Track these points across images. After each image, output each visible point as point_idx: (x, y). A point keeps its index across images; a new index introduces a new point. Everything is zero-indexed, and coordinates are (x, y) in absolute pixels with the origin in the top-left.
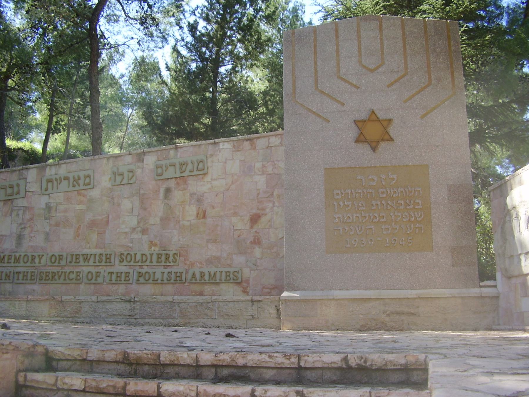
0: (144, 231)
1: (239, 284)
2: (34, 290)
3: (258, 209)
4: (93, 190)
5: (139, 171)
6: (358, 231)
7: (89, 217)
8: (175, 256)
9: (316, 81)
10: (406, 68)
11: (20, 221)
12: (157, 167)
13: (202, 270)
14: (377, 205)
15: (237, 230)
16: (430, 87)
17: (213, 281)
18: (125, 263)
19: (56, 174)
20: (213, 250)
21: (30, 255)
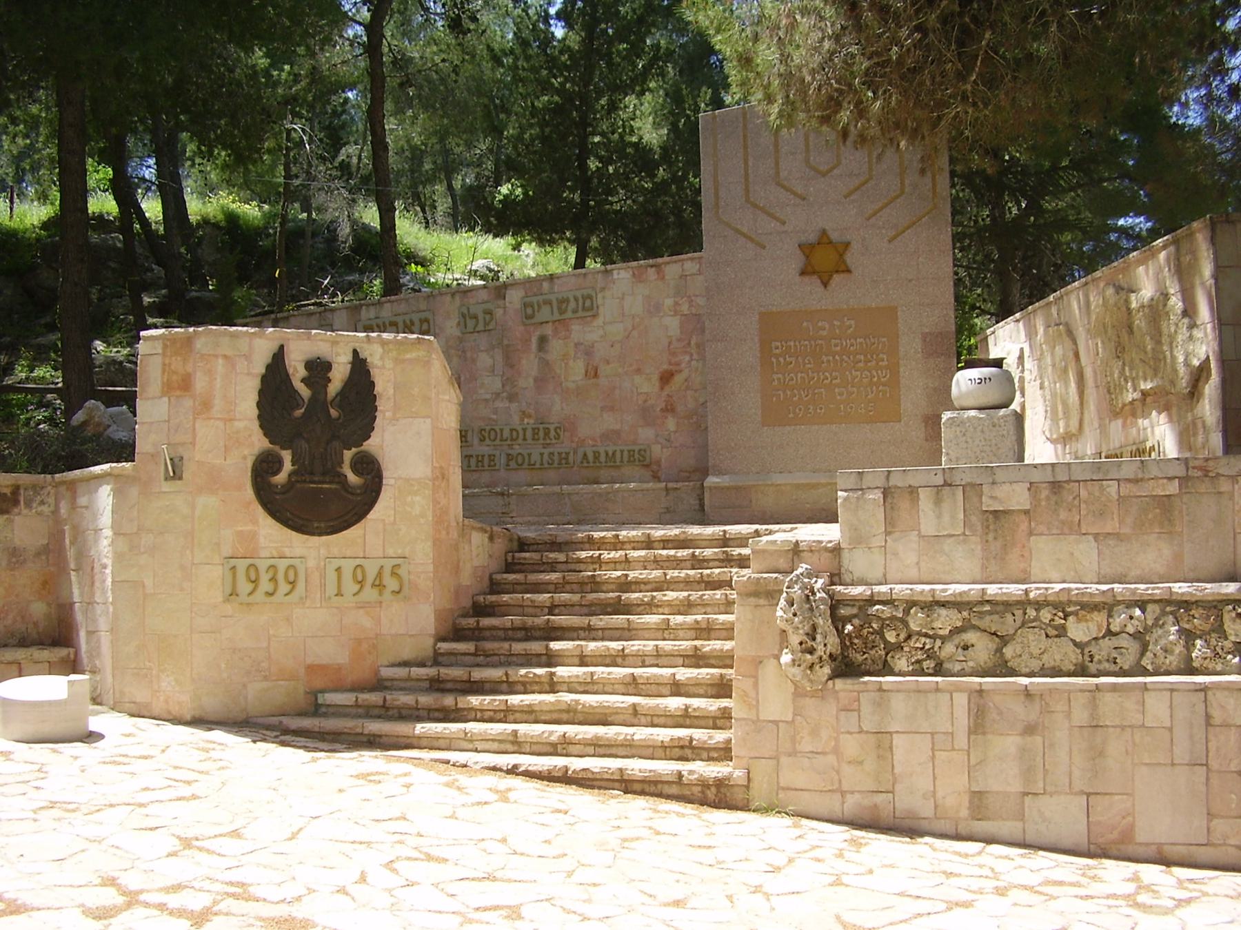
0: (512, 398)
1: (647, 466)
3: (670, 364)
9: (747, 190)
14: (829, 361)
18: (487, 442)
20: (609, 422)
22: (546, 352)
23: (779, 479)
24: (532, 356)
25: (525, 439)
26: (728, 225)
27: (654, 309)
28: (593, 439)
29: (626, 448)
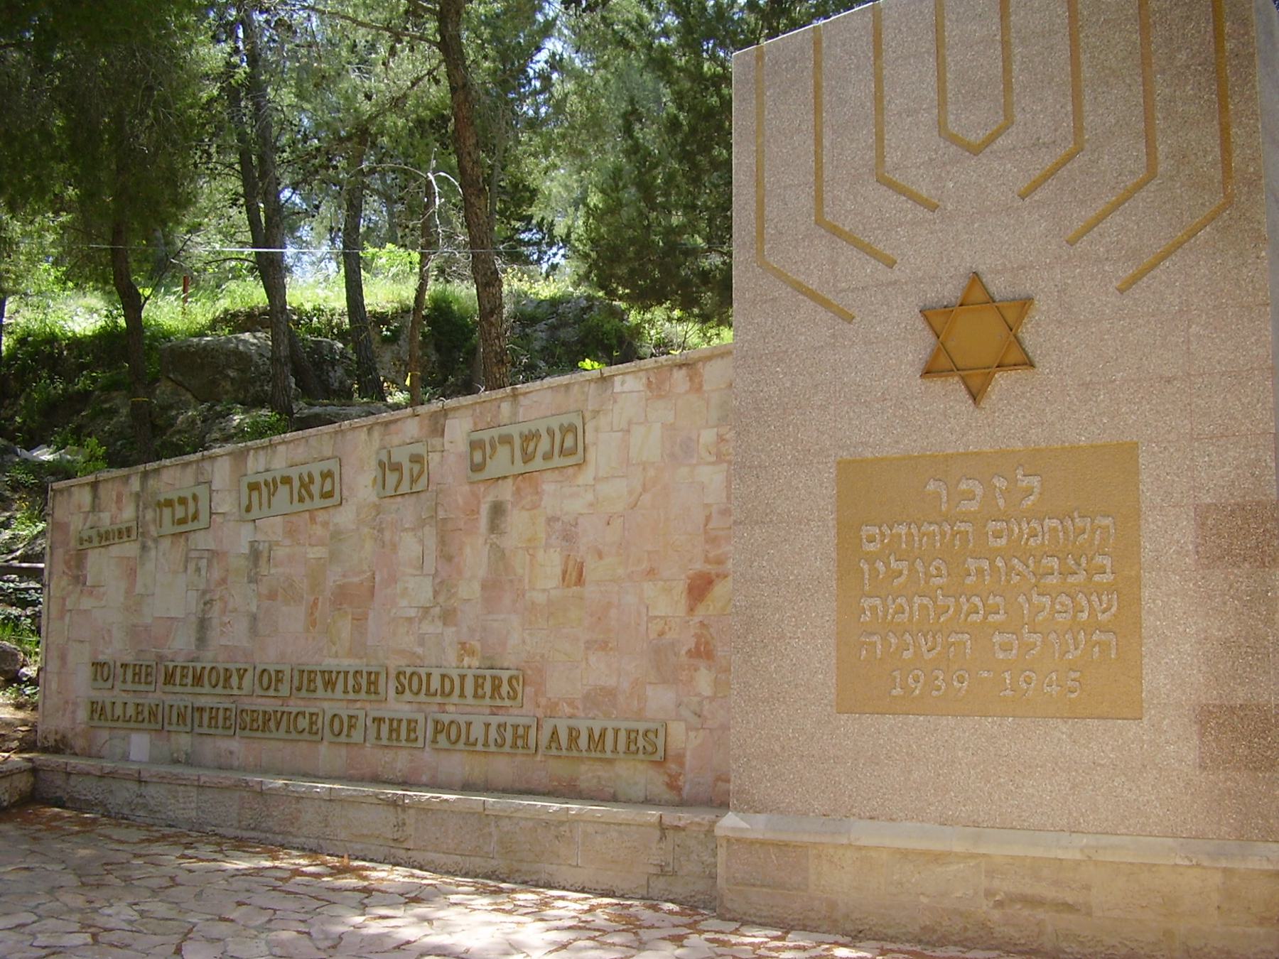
0: (448, 616)
1: (660, 764)
2: (231, 753)
3: (707, 561)
4: (341, 508)
5: (434, 458)
6: (924, 649)
7: (333, 577)
8: (514, 682)
9: (819, 199)
10: (1078, 130)
11: (202, 587)
12: (475, 445)
13: (572, 722)
14: (980, 572)
15: (656, 617)
16: (1152, 186)
17: (599, 755)
18: (408, 696)
19: (267, 470)
20: (600, 671)
21: (221, 667)
22: (502, 533)
23: (865, 834)
24: (481, 541)
25: (462, 695)
26: (780, 275)
27: (681, 449)
28: (571, 703)
29: (624, 725)
